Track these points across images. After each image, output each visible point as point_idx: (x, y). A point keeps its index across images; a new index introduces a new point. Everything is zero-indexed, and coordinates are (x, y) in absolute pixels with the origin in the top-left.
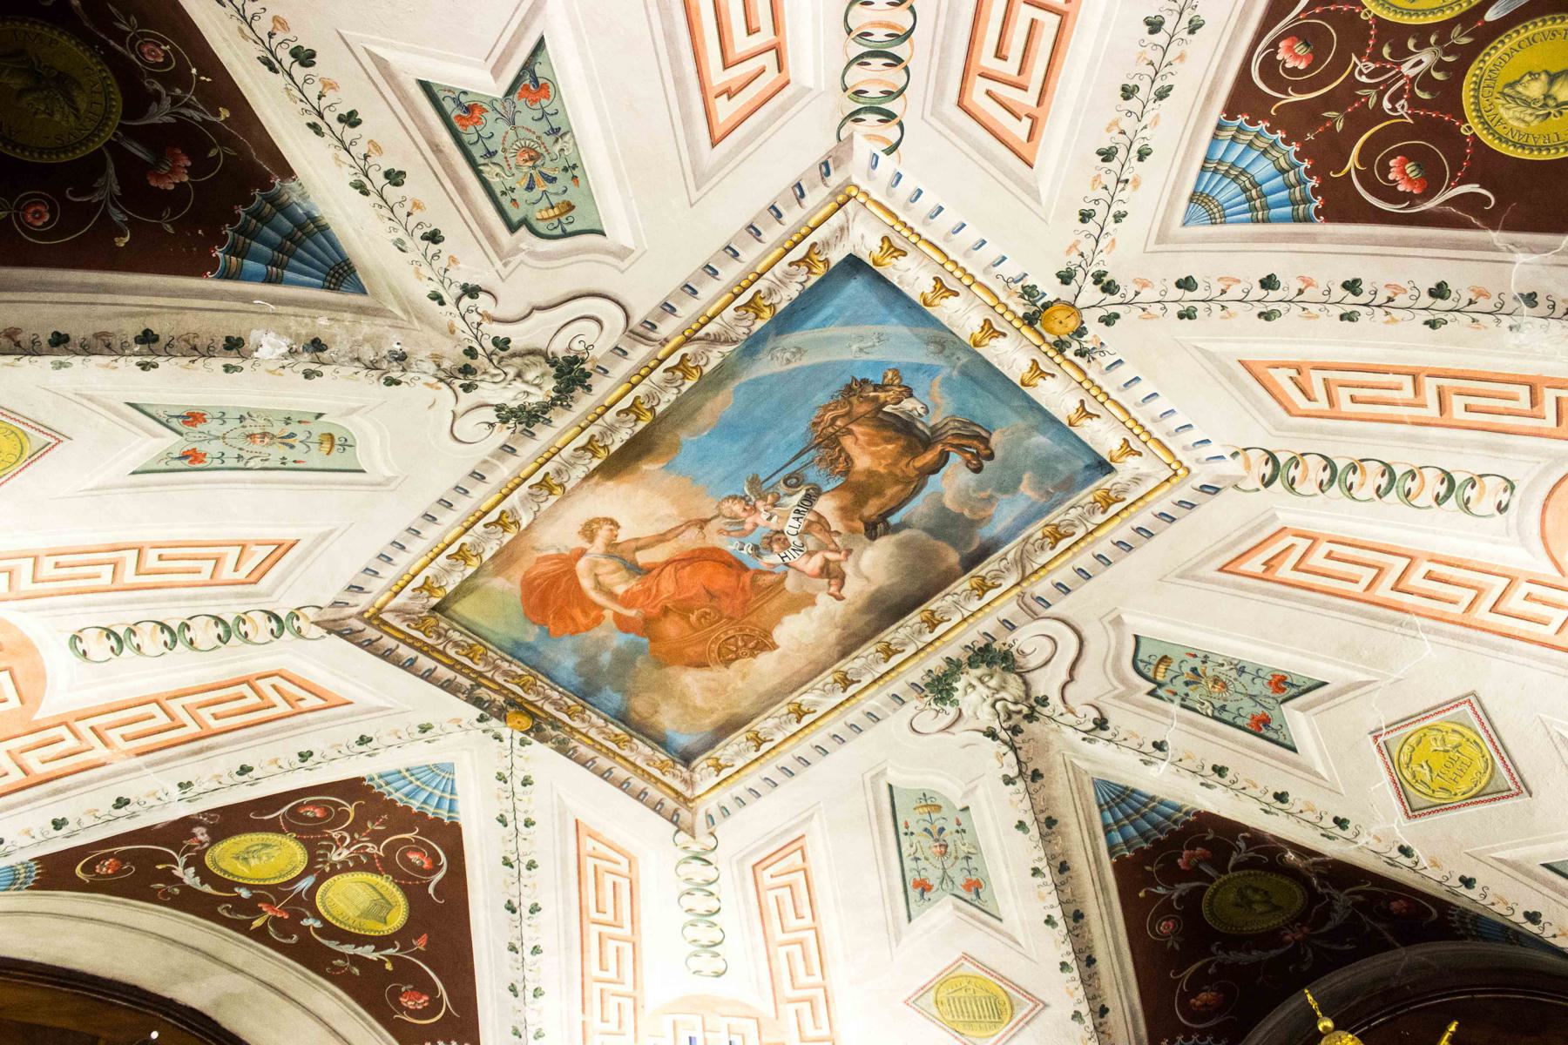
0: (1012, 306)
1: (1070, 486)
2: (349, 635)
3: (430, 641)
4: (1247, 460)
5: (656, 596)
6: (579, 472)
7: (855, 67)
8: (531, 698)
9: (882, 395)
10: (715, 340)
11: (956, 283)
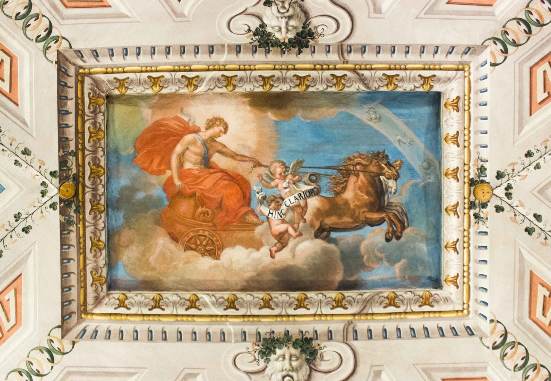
0: (471, 171)
1: (415, 282)
2: (62, 72)
3: (87, 111)
4: (495, 328)
5: (197, 184)
6: (248, 88)
7: (515, 21)
8: (88, 183)
9: (386, 169)
10: (363, 80)
11: (462, 140)
